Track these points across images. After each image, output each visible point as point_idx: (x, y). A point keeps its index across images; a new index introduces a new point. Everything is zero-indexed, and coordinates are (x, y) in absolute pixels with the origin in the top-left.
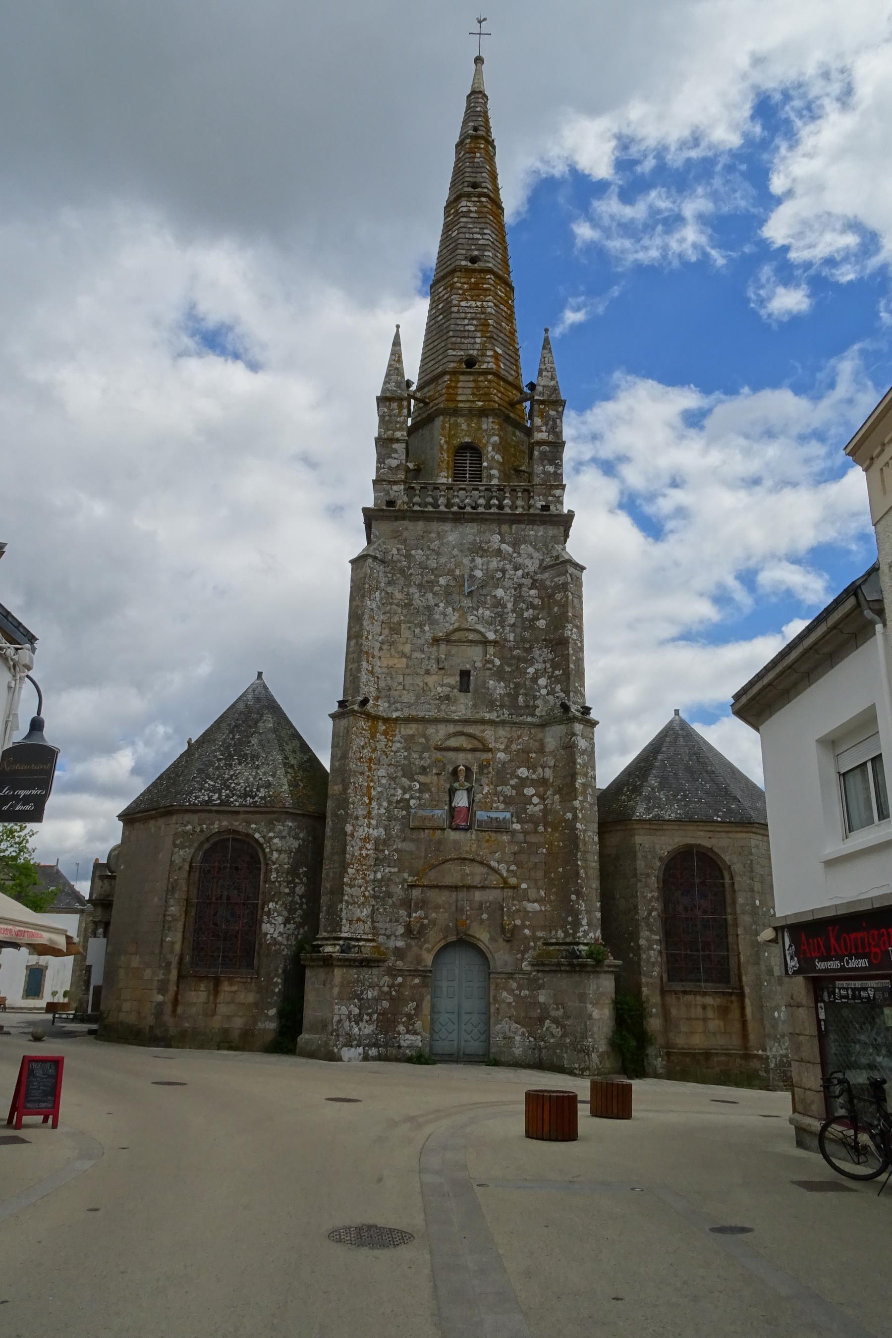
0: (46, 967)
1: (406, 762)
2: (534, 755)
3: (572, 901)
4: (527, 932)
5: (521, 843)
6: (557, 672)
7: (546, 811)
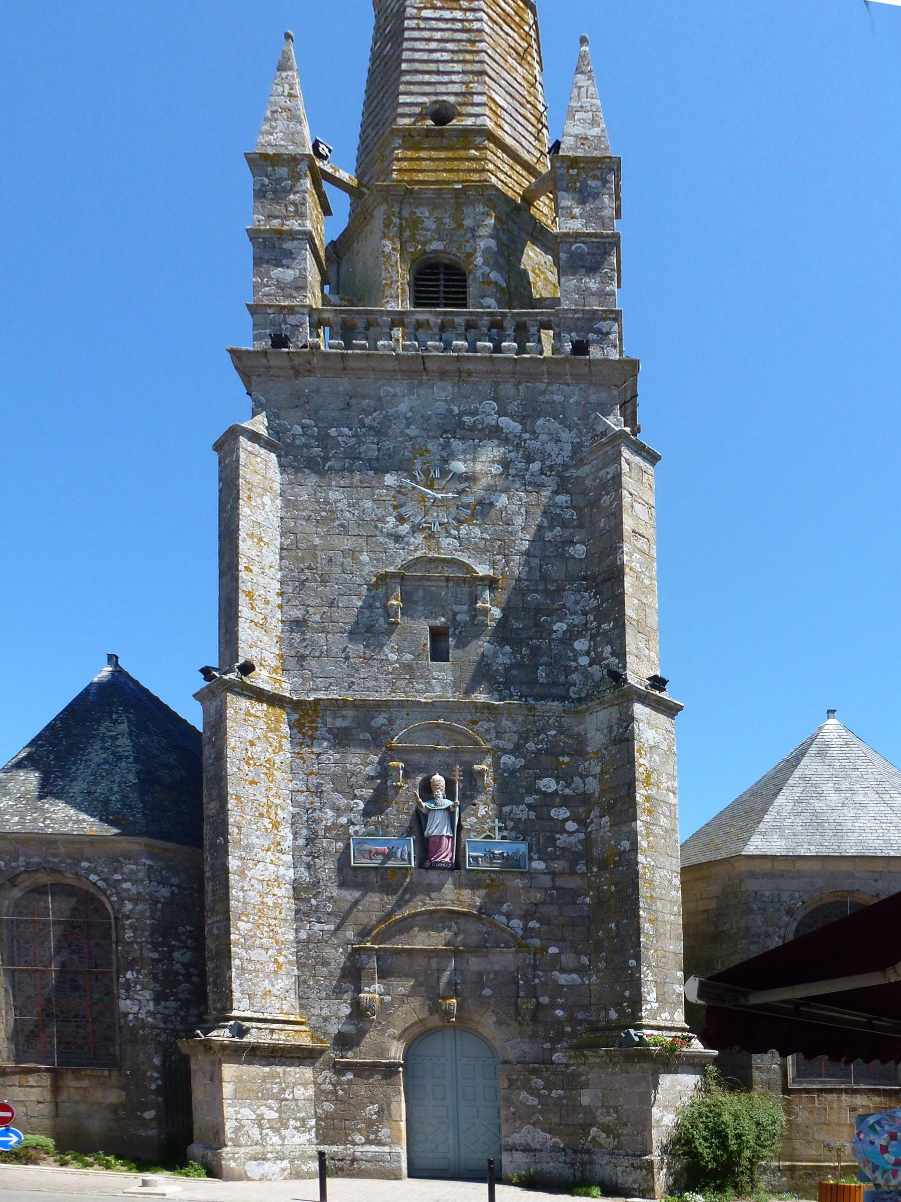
0: (213, 1171)
1: (339, 769)
2: (567, 759)
3: (631, 968)
4: (559, 1013)
5: (546, 890)
6: (605, 626)
7: (588, 842)
